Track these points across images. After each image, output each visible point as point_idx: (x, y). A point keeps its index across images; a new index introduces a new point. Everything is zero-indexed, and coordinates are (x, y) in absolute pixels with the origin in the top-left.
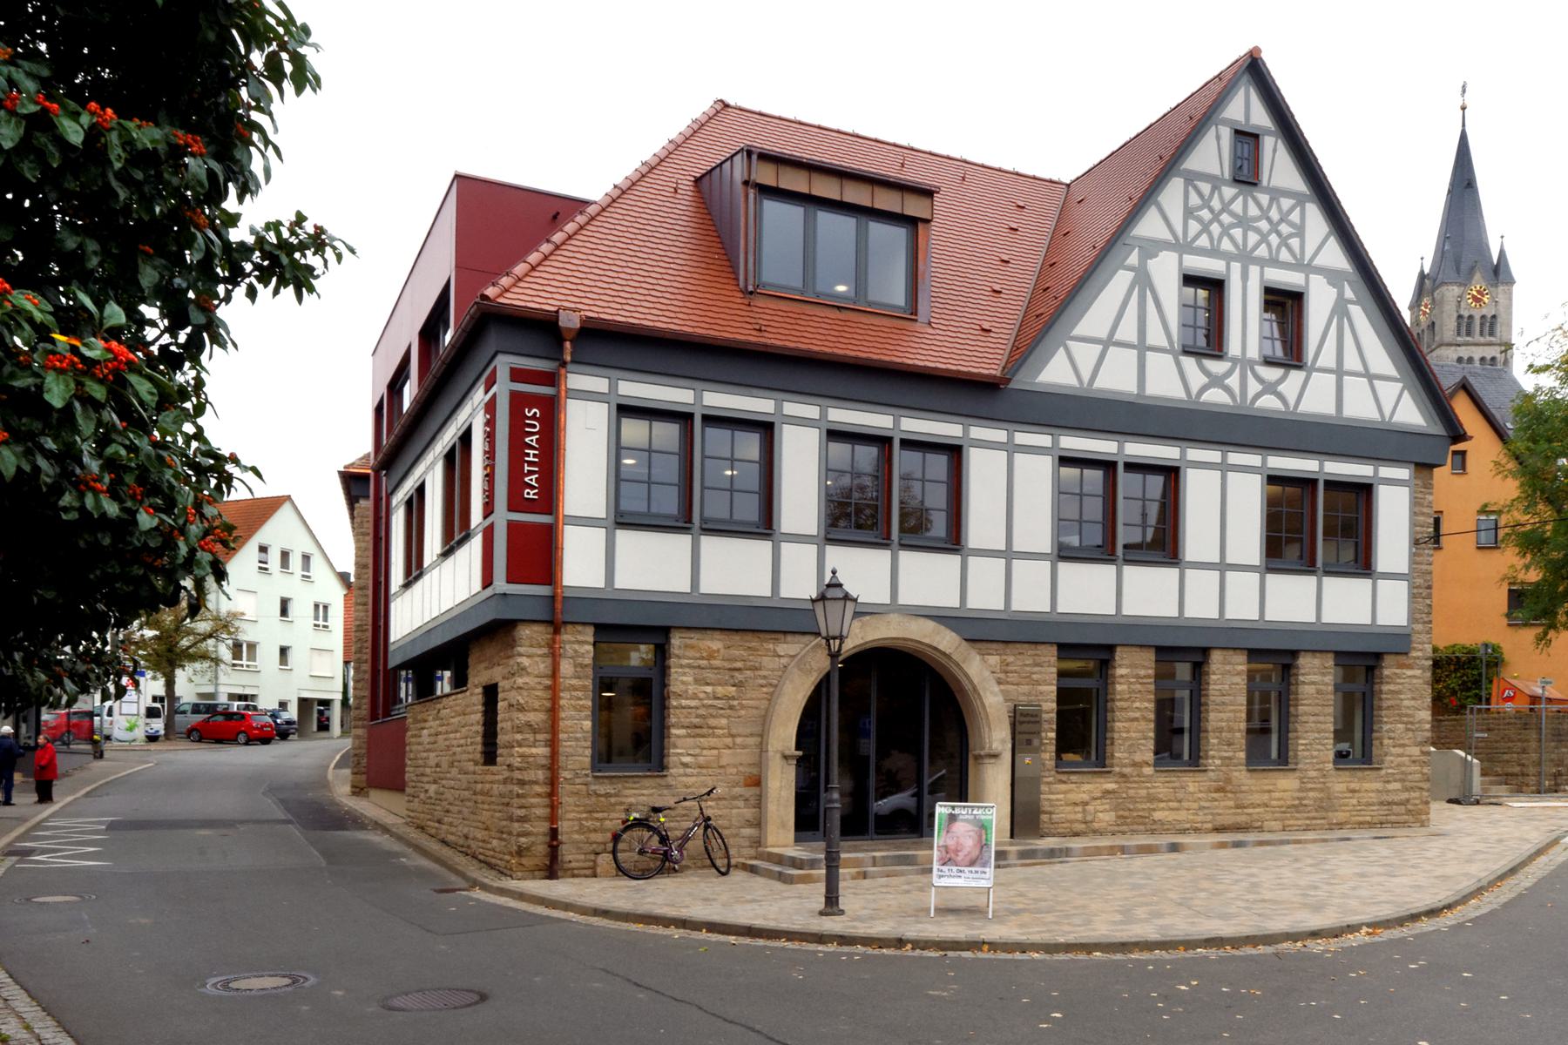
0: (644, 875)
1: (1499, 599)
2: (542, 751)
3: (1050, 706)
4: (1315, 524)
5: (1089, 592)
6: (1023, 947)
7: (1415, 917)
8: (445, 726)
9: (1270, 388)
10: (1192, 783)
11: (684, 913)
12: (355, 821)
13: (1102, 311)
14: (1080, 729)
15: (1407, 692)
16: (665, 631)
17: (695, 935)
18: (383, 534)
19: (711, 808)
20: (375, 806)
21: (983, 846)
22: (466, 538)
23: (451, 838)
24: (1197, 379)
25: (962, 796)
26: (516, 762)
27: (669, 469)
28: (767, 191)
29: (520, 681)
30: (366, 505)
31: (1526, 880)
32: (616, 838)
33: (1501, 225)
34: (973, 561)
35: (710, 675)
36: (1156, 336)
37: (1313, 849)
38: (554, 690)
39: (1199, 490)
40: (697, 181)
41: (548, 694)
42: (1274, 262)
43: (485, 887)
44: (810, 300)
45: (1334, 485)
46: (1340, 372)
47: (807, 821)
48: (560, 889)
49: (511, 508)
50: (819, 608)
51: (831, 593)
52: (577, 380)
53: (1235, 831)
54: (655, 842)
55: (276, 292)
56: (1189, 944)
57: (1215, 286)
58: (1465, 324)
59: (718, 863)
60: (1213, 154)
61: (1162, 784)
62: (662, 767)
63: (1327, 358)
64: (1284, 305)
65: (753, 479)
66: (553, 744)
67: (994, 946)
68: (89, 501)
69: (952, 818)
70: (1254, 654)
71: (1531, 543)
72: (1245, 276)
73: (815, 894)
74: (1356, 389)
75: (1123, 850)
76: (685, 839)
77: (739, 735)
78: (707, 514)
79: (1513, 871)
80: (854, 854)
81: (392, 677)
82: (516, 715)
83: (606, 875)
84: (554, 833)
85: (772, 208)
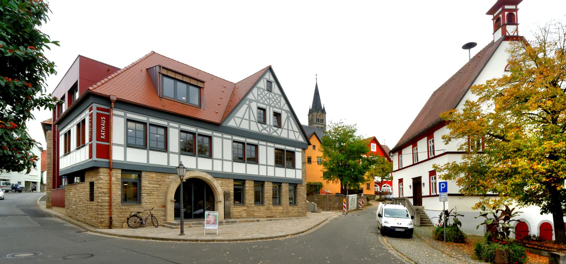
0: (136, 227)
1: (321, 174)
2: (107, 198)
3: (232, 192)
4: (284, 158)
5: (240, 169)
6: (223, 241)
7: (299, 233)
8: (78, 192)
9: (275, 131)
10: (262, 208)
11: (146, 236)
12: (50, 215)
13: (242, 111)
14: (239, 196)
15: (302, 191)
16: (141, 172)
17: (149, 240)
18: (56, 140)
19: (153, 212)
20: (55, 211)
21: (215, 220)
22: (84, 146)
23: (80, 219)
24: (261, 128)
25: (214, 210)
26: (100, 201)
27: (141, 135)
28: (164, 75)
29: (100, 182)
30: (50, 132)
31: (320, 226)
32: (128, 219)
33: (324, 102)
34: (214, 160)
35: (153, 182)
36: (252, 118)
37: (285, 221)
38: (110, 184)
39: (262, 150)
40: (147, 69)
41: (109, 185)
42: (275, 107)
43: (91, 231)
44: (175, 101)
45: (287, 151)
46: (288, 130)
47: (177, 214)
48: (113, 231)
49: (97, 140)
50: (178, 169)
51: (181, 166)
52: (115, 112)
53: (270, 217)
54: (139, 220)
55: (45, 109)
56: (257, 239)
57: (264, 110)
58: (318, 120)
59: (155, 223)
60: (262, 84)
61: (256, 208)
62: (140, 202)
63: (286, 127)
64: (277, 115)
65: (162, 138)
66: (110, 197)
67: (217, 240)
68: (5, 151)
69: (209, 215)
70: (273, 183)
71: (325, 164)
72: (270, 109)
73: (179, 231)
74: (291, 133)
75: (248, 221)
76: (147, 219)
77: (159, 196)
78: (151, 146)
79: (318, 225)
80: (187, 222)
81: (60, 179)
82: (99, 190)
83: (126, 228)
84: (111, 218)
85: (165, 79)
